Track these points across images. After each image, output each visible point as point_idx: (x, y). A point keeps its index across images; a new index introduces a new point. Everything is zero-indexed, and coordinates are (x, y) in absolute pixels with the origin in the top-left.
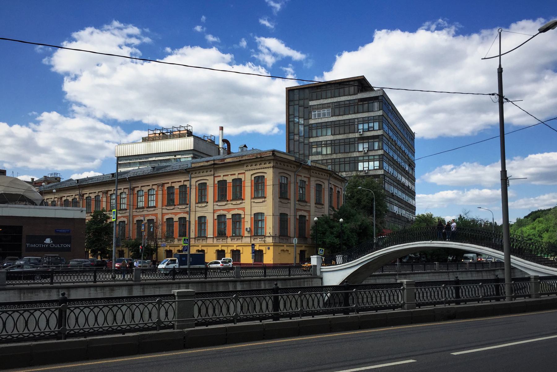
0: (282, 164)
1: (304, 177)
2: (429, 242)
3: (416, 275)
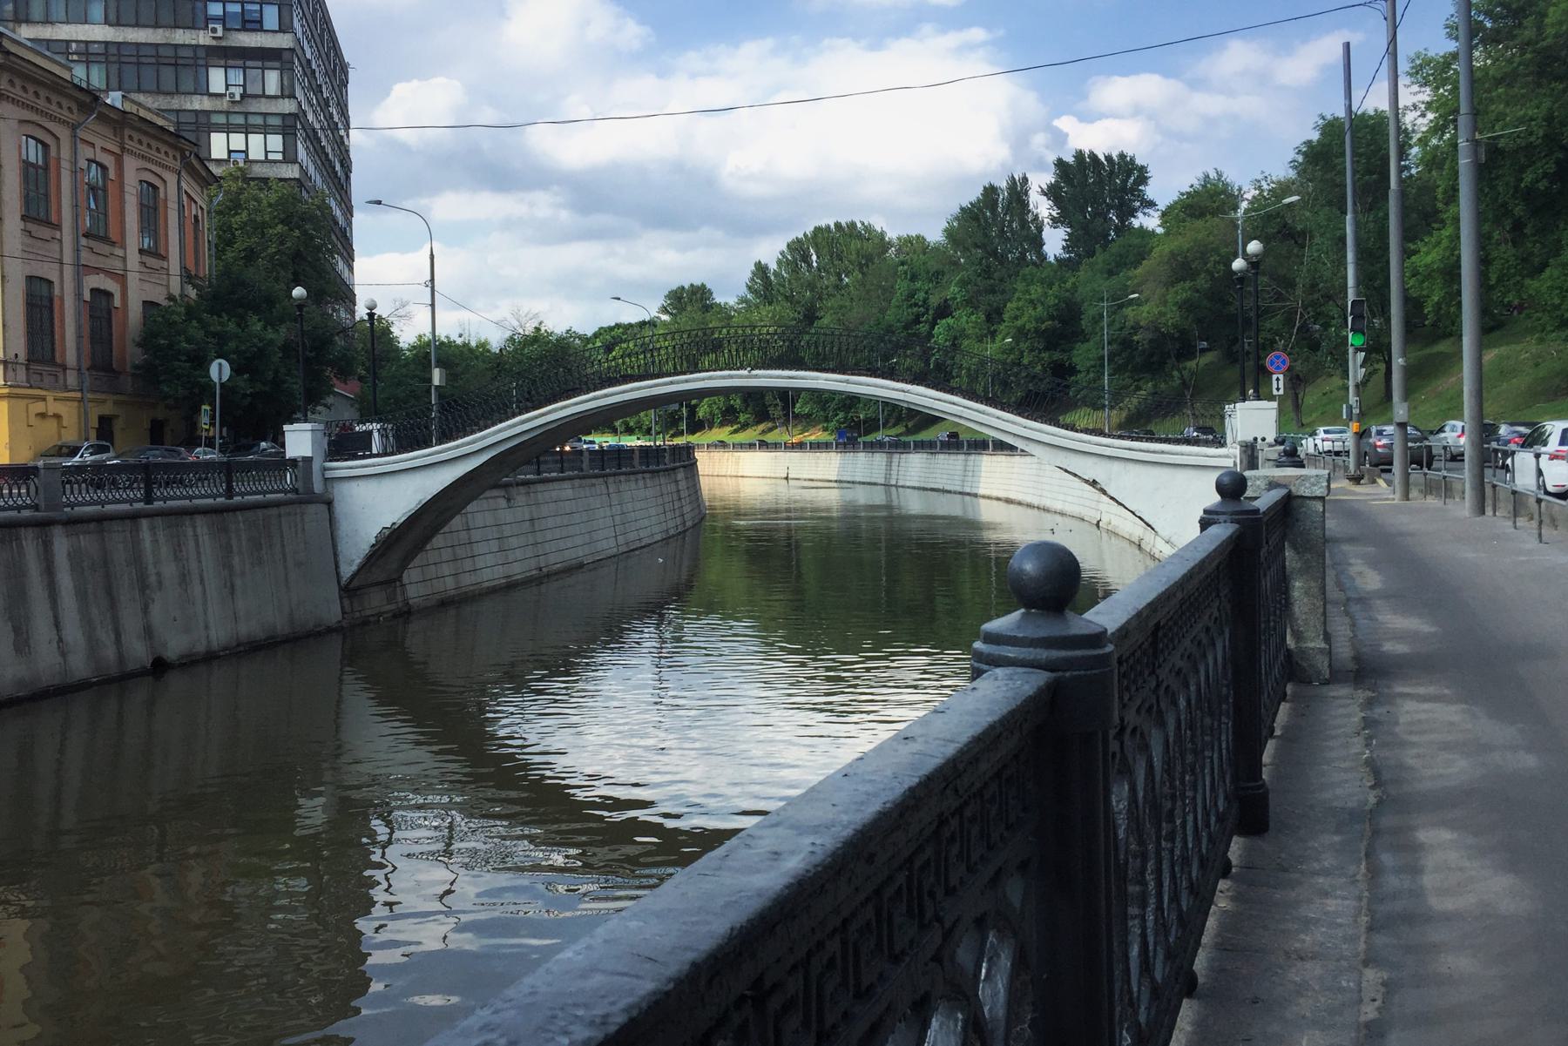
0: (31, 89)
1: (104, 149)
2: (745, 372)
3: (551, 486)
